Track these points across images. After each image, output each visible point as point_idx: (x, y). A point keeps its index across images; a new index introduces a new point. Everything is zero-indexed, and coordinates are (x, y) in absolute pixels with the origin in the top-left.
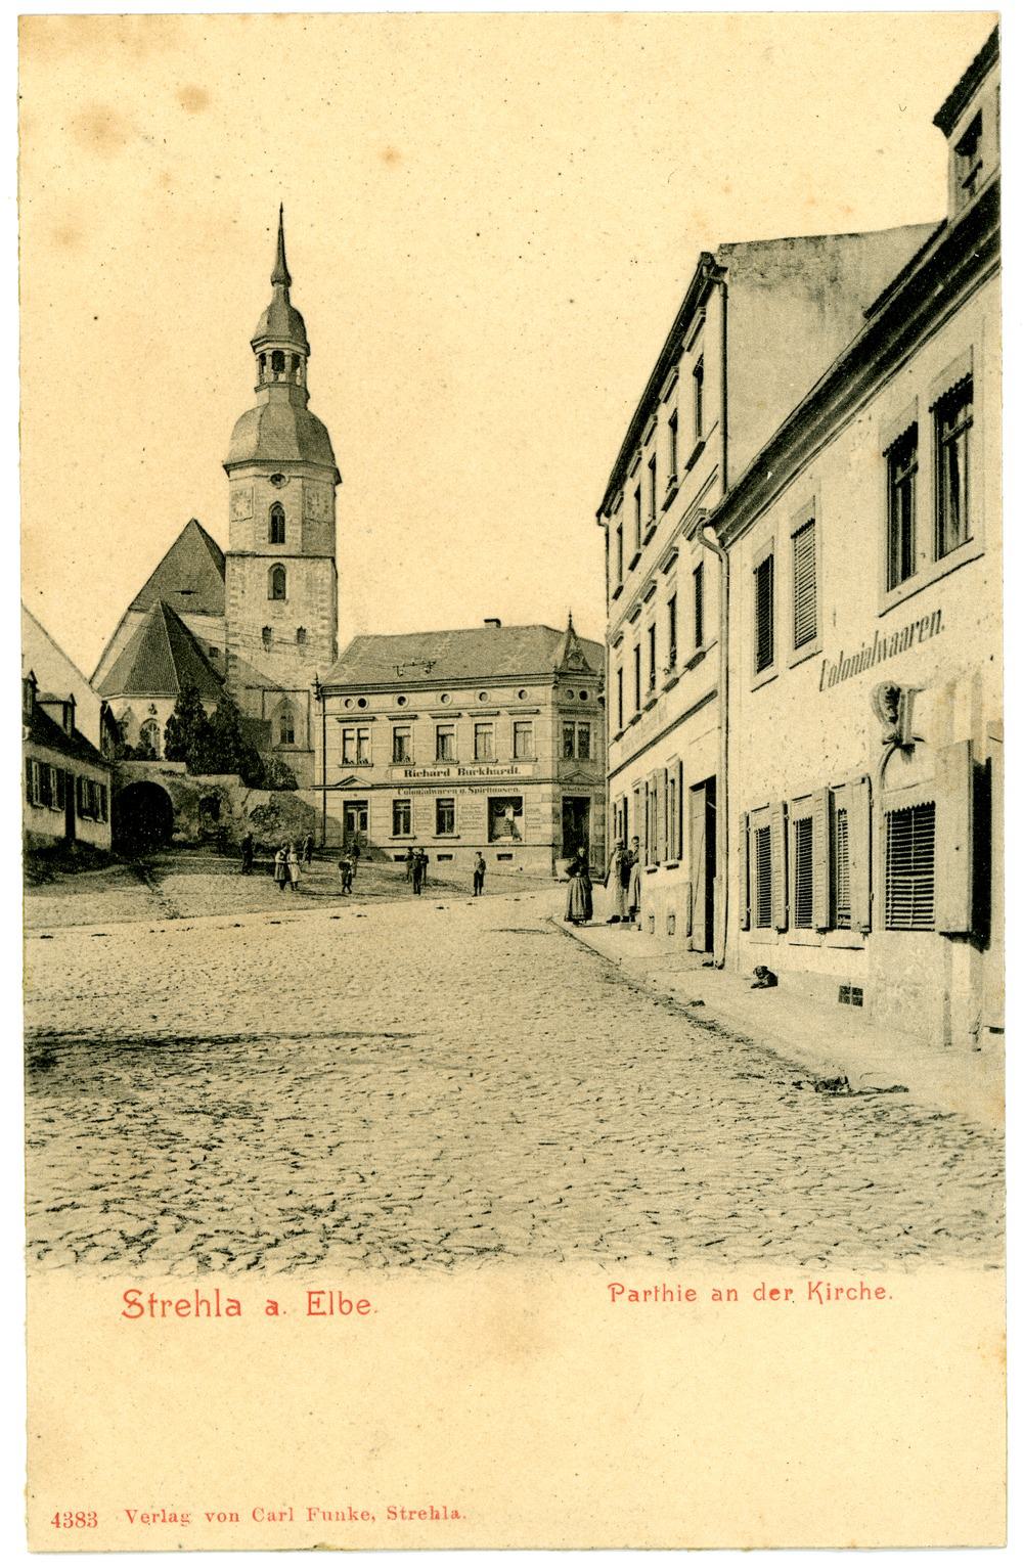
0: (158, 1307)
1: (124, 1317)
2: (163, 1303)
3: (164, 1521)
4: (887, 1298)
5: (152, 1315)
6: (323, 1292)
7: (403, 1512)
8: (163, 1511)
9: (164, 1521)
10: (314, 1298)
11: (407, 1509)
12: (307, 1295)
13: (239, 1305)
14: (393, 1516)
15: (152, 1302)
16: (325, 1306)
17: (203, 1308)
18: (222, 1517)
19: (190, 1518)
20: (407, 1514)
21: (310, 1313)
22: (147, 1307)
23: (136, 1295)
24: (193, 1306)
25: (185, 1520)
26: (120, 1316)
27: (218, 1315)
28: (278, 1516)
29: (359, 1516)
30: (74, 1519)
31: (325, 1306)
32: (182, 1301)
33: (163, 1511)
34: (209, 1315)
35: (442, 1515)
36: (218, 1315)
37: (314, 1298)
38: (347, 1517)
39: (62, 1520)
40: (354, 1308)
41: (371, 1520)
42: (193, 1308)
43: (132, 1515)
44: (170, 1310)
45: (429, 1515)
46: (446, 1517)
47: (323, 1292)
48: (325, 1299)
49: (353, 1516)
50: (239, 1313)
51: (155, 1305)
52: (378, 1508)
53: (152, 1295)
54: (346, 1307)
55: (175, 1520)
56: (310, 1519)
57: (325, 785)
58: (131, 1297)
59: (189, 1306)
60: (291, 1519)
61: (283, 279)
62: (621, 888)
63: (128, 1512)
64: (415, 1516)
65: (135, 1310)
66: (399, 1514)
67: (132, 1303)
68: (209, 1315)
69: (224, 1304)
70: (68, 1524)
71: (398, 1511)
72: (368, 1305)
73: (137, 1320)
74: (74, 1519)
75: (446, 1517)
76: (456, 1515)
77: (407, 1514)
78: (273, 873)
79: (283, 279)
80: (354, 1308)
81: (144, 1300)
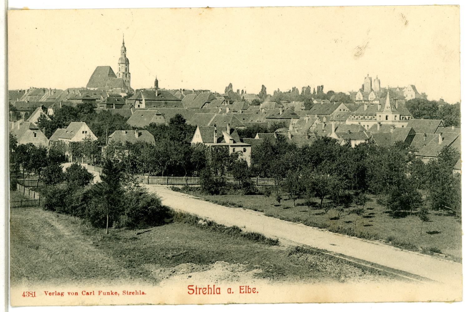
4: (256, 293)
7: (127, 292)
8: (56, 292)
11: (129, 292)
12: (221, 293)
15: (196, 288)
19: (63, 294)
20: (129, 293)
25: (99, 292)
28: (89, 293)
29: (114, 293)
33: (56, 292)
35: (139, 293)
38: (110, 293)
41: (118, 295)
43: (46, 292)
46: (140, 294)
49: (112, 294)
55: (60, 295)
57: (168, 183)
60: (94, 294)
61: (124, 44)
62: (410, 96)
63: (45, 292)
64: (131, 294)
66: (126, 293)
71: (126, 292)
75: (140, 294)
76: (143, 293)
78: (101, 148)
79: (124, 44)
81: (194, 288)
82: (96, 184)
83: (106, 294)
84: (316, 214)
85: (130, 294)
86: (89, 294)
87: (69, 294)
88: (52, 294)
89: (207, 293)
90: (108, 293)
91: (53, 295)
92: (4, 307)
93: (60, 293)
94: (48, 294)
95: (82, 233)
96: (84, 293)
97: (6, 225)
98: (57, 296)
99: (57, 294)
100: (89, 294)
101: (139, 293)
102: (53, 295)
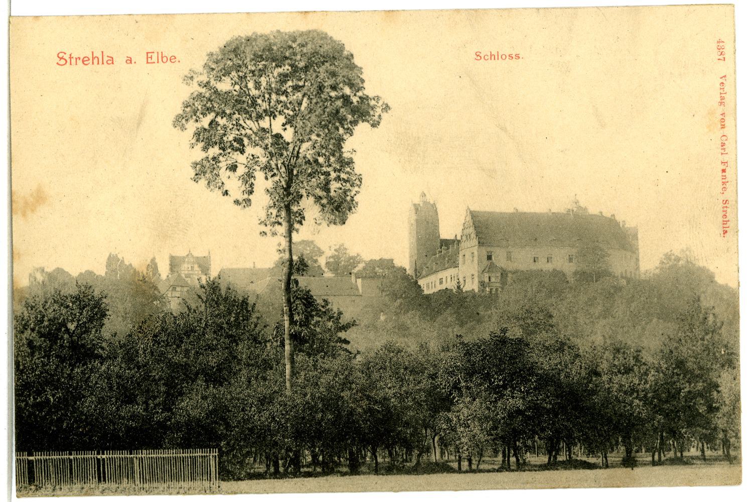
0: (73, 61)
1: (58, 66)
2: (76, 59)
3: (721, 93)
5: (71, 64)
6: (153, 52)
7: (726, 207)
8: (726, 93)
9: (721, 93)
10: (150, 55)
13: (112, 58)
14: (725, 202)
15: (71, 58)
16: (155, 59)
17: (96, 61)
18: (723, 121)
20: (725, 209)
21: (147, 63)
22: (69, 61)
23: (63, 54)
24: (91, 59)
26: (56, 64)
27: (103, 63)
30: (721, 50)
31: (155, 59)
32: (85, 57)
33: (726, 93)
34: (98, 64)
35: (725, 226)
36: (103, 63)
37: (150, 55)
38: (724, 181)
39: (721, 44)
40: (169, 60)
42: (91, 61)
44: (80, 62)
45: (725, 220)
47: (153, 52)
48: (155, 56)
49: (724, 183)
50: (113, 63)
51: (72, 59)
52: (729, 195)
53: (70, 55)
54: (165, 59)
56: (722, 163)
58: (61, 55)
59: (89, 60)
65: (63, 62)
66: (725, 205)
67: (61, 58)
68: (98, 64)
69: (106, 59)
70: (720, 47)
72: (175, 58)
73: (60, 66)
74: (721, 50)
75: (723, 227)
77: (725, 209)
80: (169, 60)
81: (67, 57)
82: (344, 414)
83: (724, 174)
84: (447, 282)
85: (723, 211)
86: (722, 146)
87: (722, 115)
88: (722, 87)
89: (91, 63)
90: (724, 177)
91: (721, 89)
92: (6, 496)
93: (723, 101)
94: (721, 81)
95: (607, 336)
96: (724, 138)
97: (148, 492)
98: (719, 96)
99: (723, 95)
100: (722, 146)
101: (725, 226)
102: (721, 89)
